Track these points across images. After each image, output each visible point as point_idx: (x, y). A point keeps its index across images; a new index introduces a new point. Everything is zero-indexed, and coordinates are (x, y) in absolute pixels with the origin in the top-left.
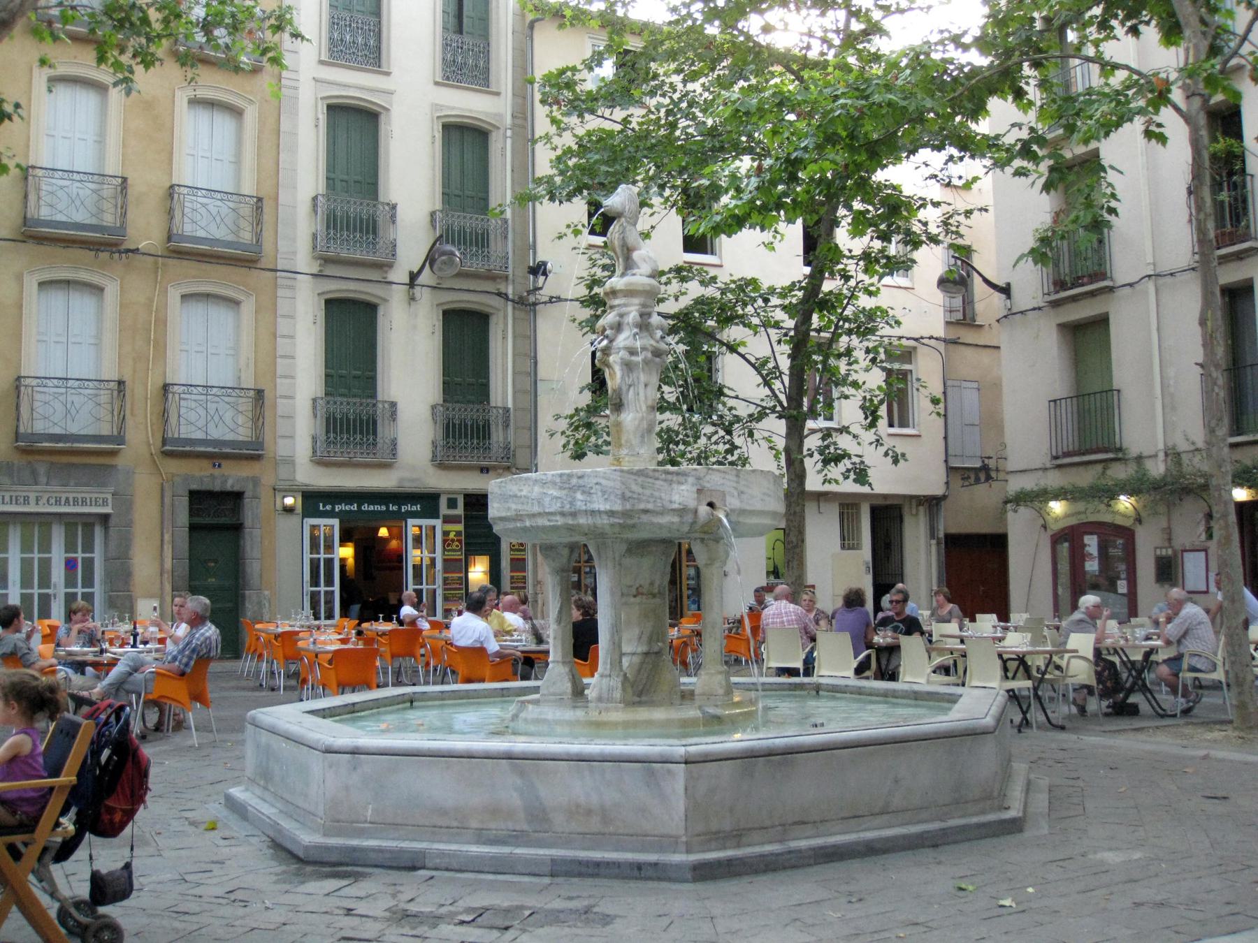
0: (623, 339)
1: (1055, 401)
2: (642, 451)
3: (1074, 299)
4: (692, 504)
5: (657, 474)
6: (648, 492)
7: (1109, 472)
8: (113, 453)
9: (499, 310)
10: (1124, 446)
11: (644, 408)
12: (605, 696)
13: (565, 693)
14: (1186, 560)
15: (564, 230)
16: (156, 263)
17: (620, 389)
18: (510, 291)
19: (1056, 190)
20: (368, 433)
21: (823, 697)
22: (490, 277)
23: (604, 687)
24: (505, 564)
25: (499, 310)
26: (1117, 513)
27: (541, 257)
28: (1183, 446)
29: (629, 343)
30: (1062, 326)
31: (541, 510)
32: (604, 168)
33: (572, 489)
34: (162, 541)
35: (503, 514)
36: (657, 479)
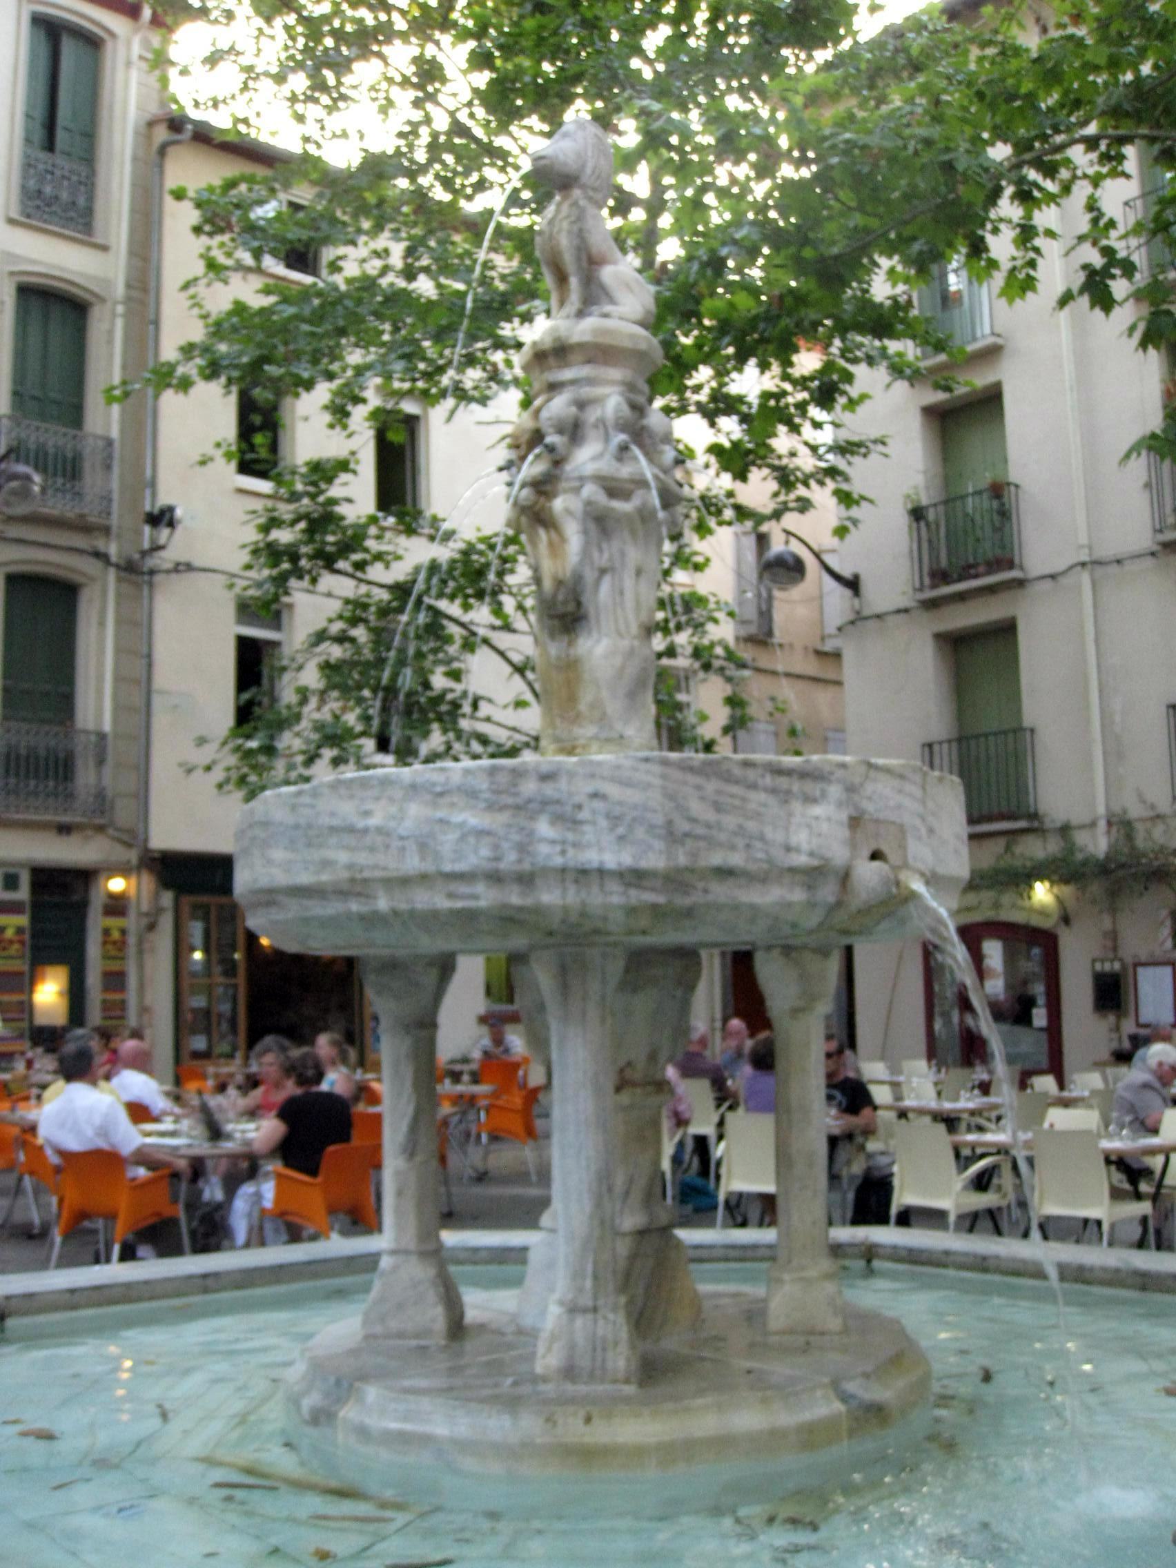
0: (588, 458)
1: (930, 746)
2: (630, 731)
3: (961, 597)
4: (838, 853)
5: (751, 775)
6: (730, 821)
7: (1018, 850)
9: (93, 579)
10: (1041, 812)
11: (634, 629)
12: (584, 1362)
13: (425, 1333)
14: (1140, 978)
15: (210, 450)
17: (578, 578)
18: (113, 550)
19: (1157, 347)
21: (884, 1275)
22: (83, 527)
23: (580, 1339)
24: (93, 979)
25: (93, 579)
26: (1032, 910)
27: (164, 500)
28: (1135, 811)
29: (607, 466)
30: (940, 637)
31: (429, 867)
32: (306, 327)
33: (526, 809)
35: (305, 878)
36: (753, 786)
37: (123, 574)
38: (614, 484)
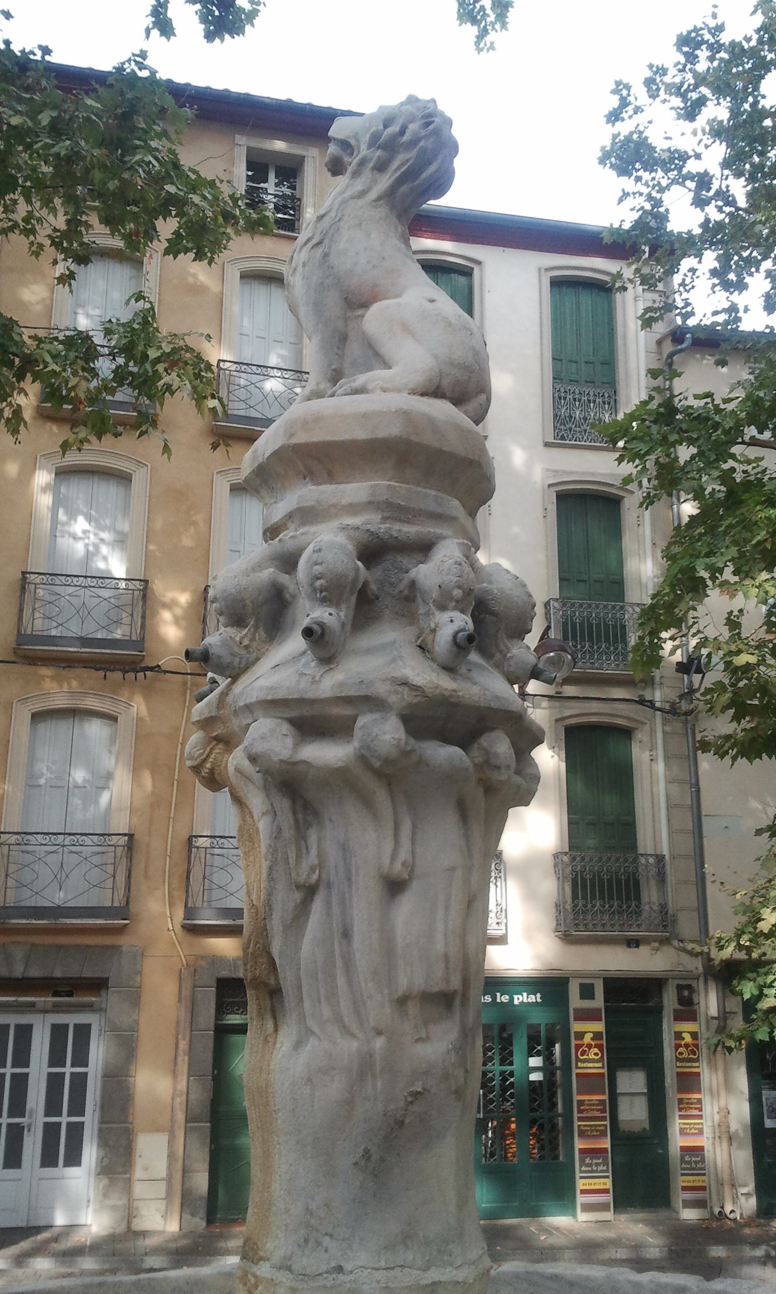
8: (120, 931)
16: (185, 683)
18: (658, 696)
20: (628, 898)
24: (670, 1080)
25: (643, 723)
34: (177, 1048)
37: (669, 716)
38: (305, 711)
